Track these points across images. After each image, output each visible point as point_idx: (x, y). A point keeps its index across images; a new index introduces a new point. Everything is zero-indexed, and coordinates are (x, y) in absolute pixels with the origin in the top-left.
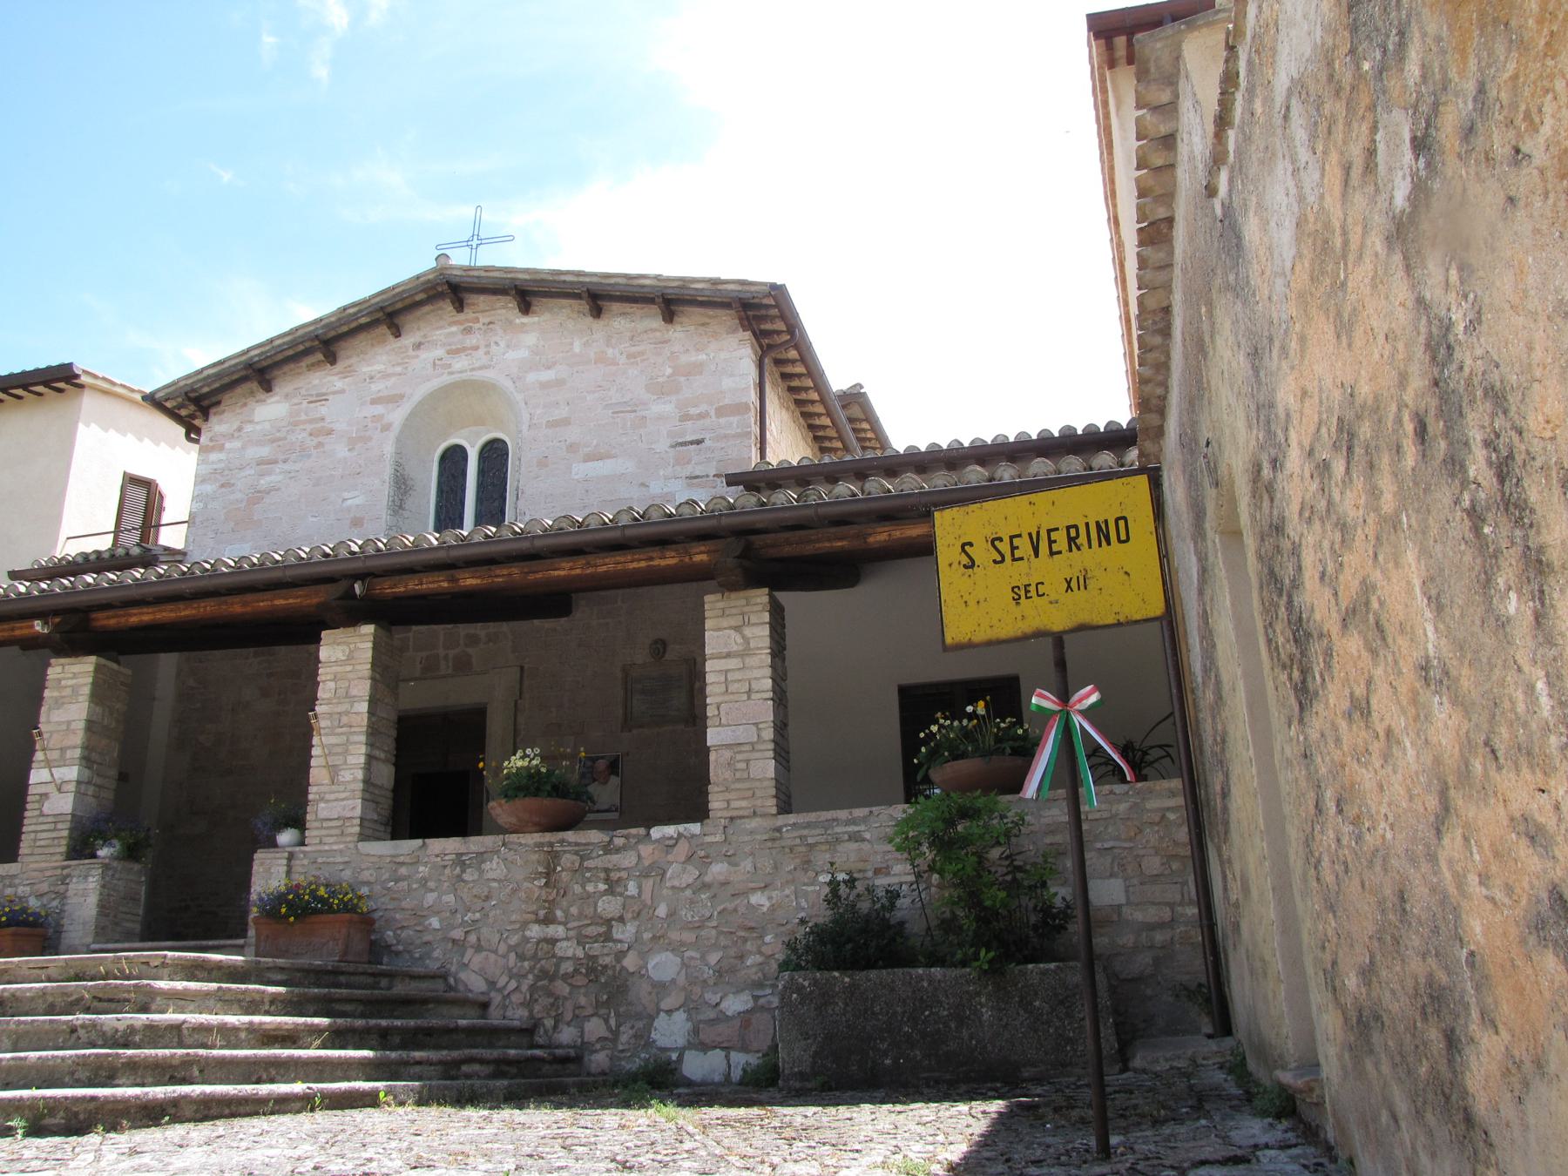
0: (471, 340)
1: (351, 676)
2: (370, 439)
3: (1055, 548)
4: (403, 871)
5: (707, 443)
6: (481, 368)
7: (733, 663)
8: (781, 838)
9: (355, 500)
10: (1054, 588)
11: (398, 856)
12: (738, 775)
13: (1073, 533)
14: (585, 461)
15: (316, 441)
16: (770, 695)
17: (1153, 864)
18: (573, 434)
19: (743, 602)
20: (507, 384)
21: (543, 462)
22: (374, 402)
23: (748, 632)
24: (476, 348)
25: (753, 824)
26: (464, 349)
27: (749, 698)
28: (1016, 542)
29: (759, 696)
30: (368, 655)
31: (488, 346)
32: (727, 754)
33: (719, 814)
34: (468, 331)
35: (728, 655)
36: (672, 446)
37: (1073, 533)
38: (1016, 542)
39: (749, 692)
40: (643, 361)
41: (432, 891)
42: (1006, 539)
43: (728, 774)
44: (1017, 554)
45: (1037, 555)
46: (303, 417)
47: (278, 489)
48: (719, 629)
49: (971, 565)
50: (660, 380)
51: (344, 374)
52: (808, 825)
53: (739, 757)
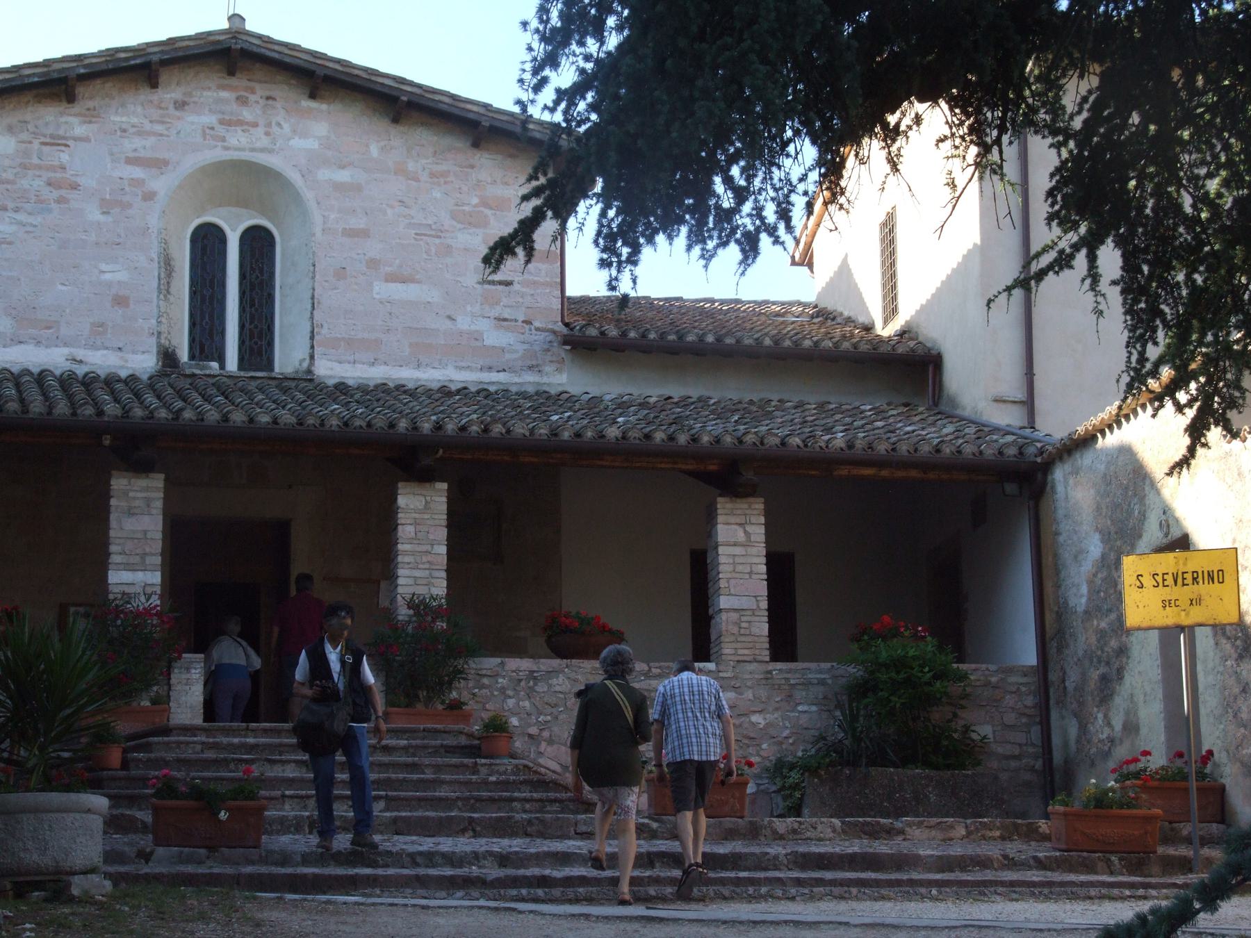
0: (247, 114)
1: (429, 522)
2: (130, 205)
3: (1186, 582)
4: (486, 681)
5: (516, 287)
6: (262, 150)
7: (738, 550)
8: (772, 678)
9: (116, 274)
10: (1185, 602)
11: (481, 669)
12: (742, 631)
13: (1195, 575)
14: (387, 281)
15: (56, 194)
16: (765, 577)
17: (1010, 718)
18: (373, 248)
19: (746, 506)
20: (294, 176)
21: (341, 273)
22: (130, 161)
23: (749, 528)
24: (255, 125)
25: (753, 666)
26: (240, 123)
27: (750, 577)
28: (1166, 577)
29: (758, 576)
30: (444, 507)
31: (269, 125)
32: (734, 616)
33: (730, 658)
34: (242, 101)
35: (735, 544)
36: (479, 283)
37: (1195, 575)
38: (1166, 577)
39: (750, 573)
40: (446, 183)
41: (510, 697)
42: (1161, 575)
43: (735, 630)
44: (1166, 583)
45: (1176, 585)
46: (35, 161)
47: (10, 243)
48: (728, 524)
49: (1142, 587)
50: (466, 208)
51: (90, 116)
52: (789, 671)
53: (744, 619)
